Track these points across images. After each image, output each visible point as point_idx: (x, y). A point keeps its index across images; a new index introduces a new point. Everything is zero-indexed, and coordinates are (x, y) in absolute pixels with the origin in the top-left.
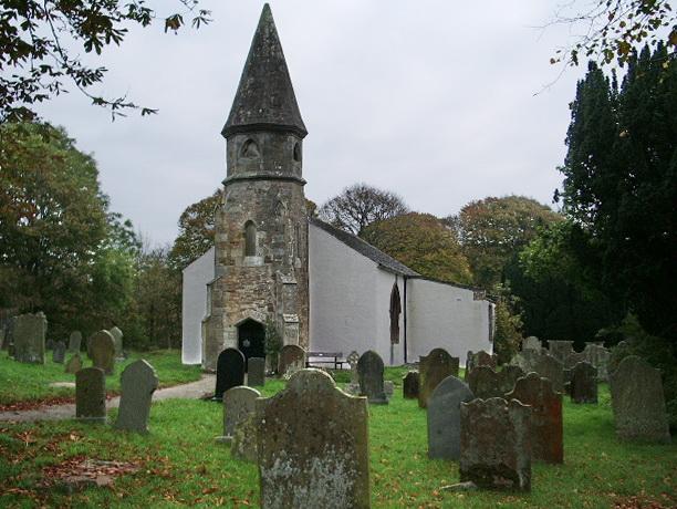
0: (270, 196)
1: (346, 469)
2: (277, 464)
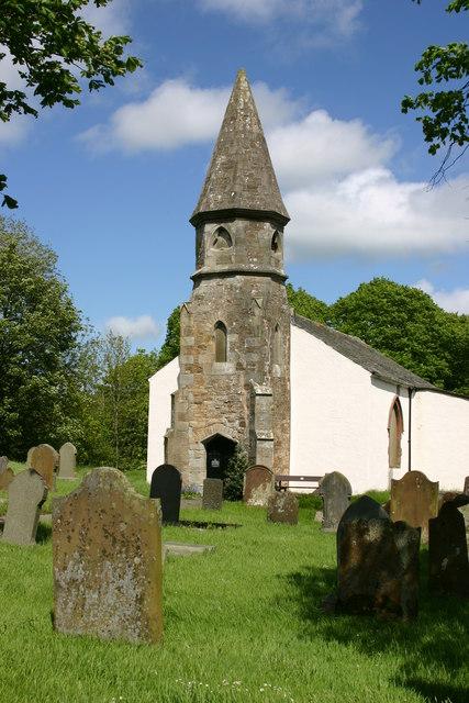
0: (242, 292)
1: (135, 575)
2: (70, 566)
